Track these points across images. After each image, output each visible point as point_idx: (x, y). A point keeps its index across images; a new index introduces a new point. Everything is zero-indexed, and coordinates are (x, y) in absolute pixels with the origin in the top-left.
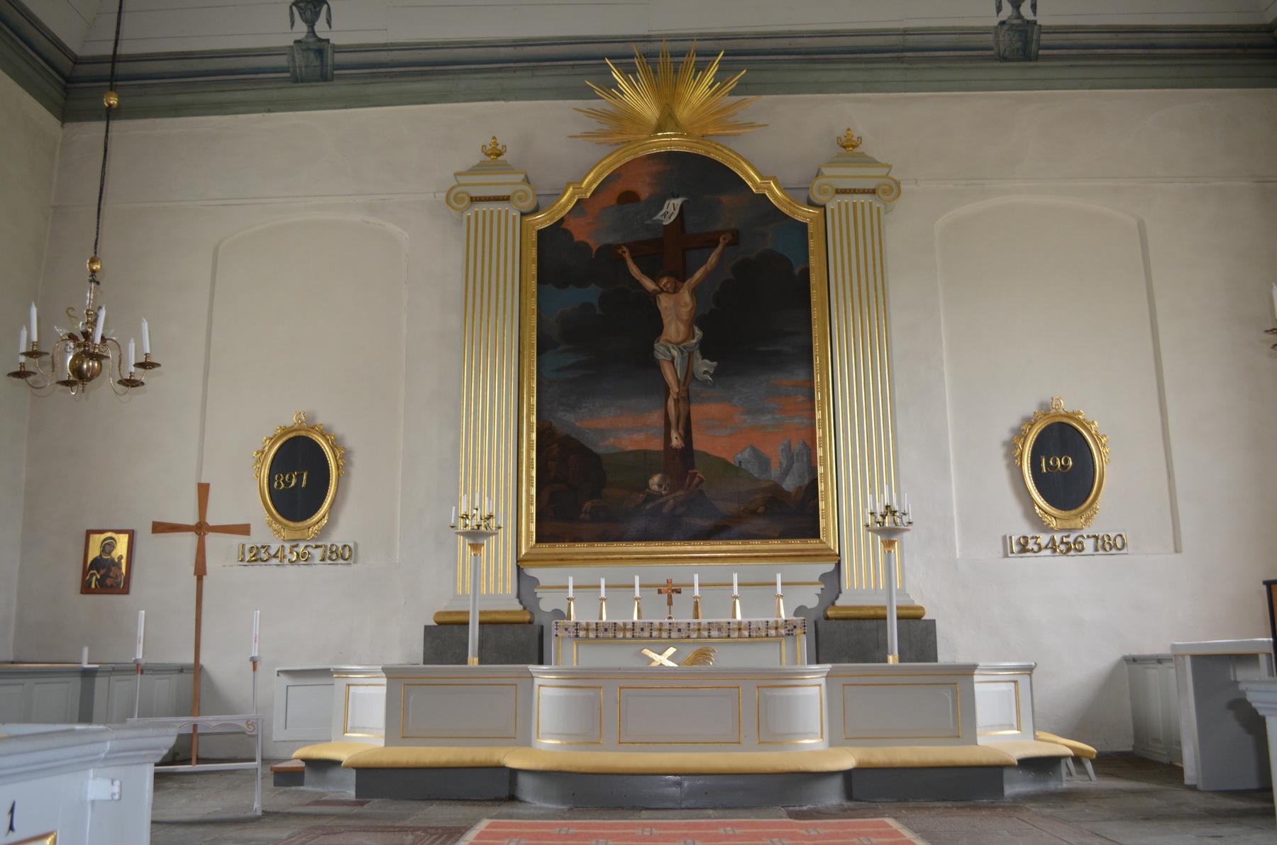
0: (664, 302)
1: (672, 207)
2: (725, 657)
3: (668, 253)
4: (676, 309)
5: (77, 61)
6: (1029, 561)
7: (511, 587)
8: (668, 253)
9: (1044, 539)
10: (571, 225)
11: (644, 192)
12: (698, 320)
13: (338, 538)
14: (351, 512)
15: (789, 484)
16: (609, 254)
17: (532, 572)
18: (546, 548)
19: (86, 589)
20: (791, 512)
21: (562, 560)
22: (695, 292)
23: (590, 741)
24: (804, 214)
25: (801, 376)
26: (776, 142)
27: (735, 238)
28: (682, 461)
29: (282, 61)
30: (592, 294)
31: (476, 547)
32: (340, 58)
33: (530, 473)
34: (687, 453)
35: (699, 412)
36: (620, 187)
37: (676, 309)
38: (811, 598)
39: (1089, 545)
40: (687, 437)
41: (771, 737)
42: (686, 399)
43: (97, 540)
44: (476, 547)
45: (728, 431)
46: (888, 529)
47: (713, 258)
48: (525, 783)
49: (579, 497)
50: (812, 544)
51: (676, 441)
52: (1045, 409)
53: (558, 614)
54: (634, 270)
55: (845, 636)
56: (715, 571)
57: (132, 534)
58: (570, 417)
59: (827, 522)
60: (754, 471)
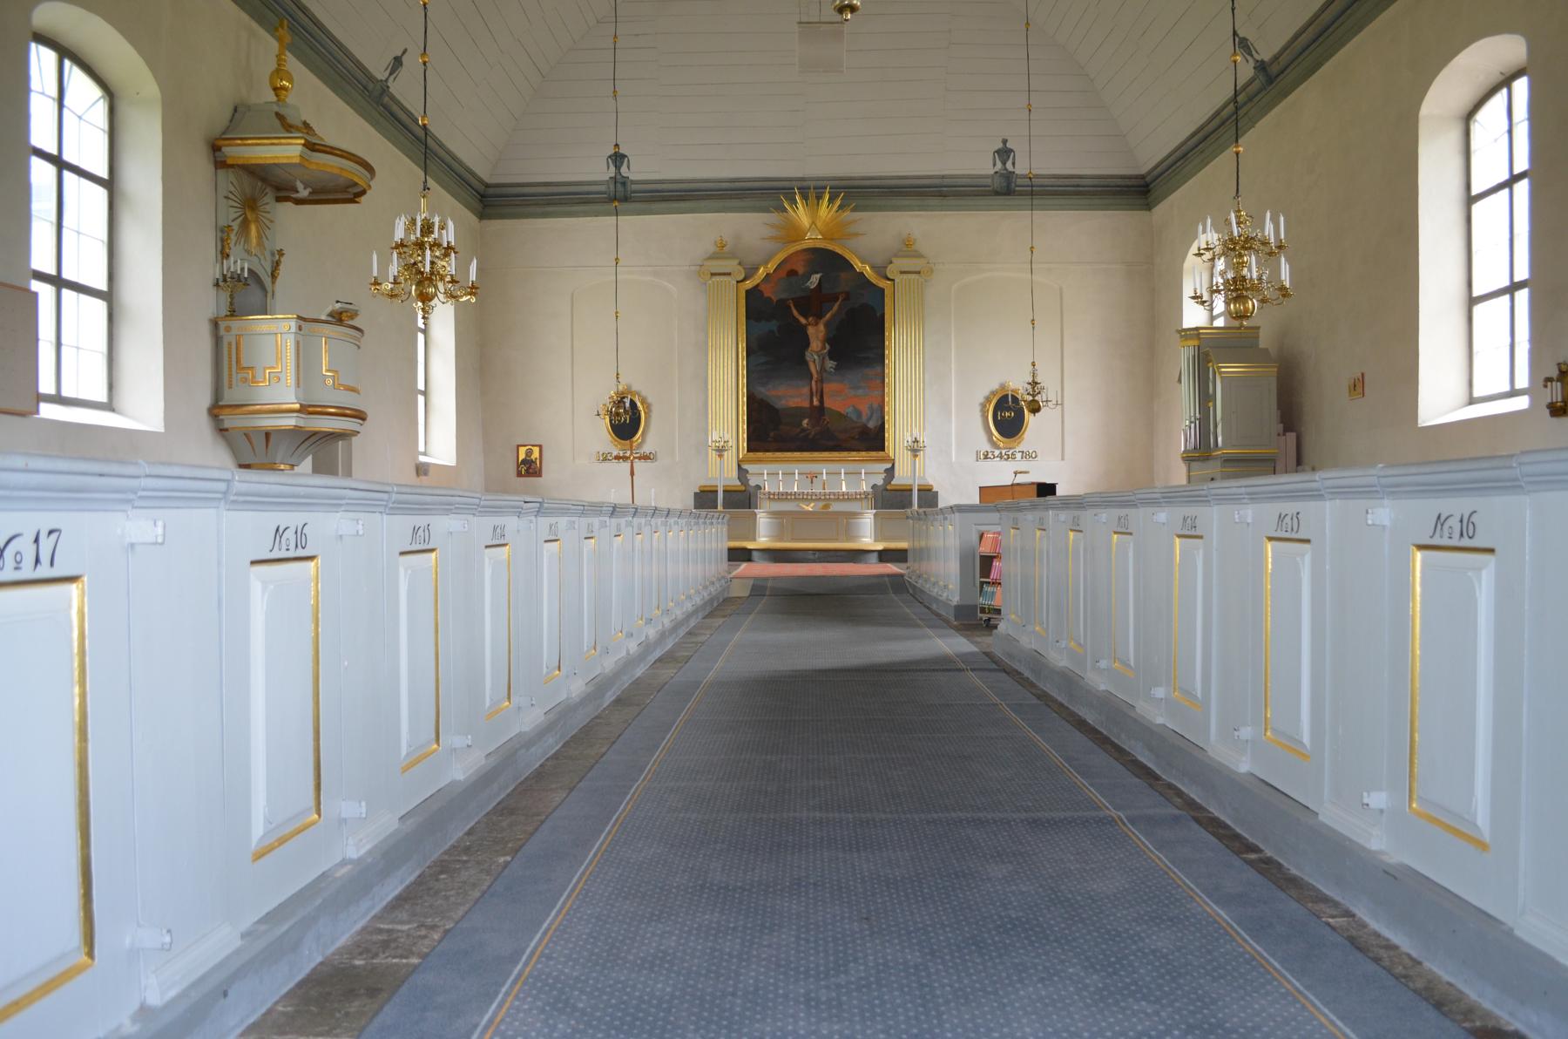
0: (811, 331)
1: (815, 278)
2: (836, 507)
3: (813, 304)
4: (817, 334)
5: (487, 186)
6: (988, 463)
7: (735, 474)
8: (813, 304)
9: (997, 453)
10: (762, 288)
11: (801, 270)
12: (828, 340)
13: (646, 449)
14: (651, 438)
15: (871, 425)
16: (782, 302)
17: (745, 466)
18: (751, 454)
19: (519, 474)
20: (871, 439)
21: (760, 461)
22: (827, 325)
23: (781, 540)
24: (882, 283)
25: (879, 369)
26: (871, 238)
27: (847, 296)
28: (819, 412)
29: (603, 188)
30: (773, 325)
31: (721, 456)
32: (634, 187)
33: (743, 418)
34: (821, 408)
35: (827, 388)
36: (788, 267)
37: (817, 334)
38: (879, 480)
39: (1019, 456)
40: (821, 401)
41: (851, 537)
42: (821, 381)
43: (523, 451)
44: (721, 456)
45: (841, 398)
46: (915, 449)
47: (836, 307)
48: (755, 554)
49: (769, 430)
50: (881, 454)
51: (816, 403)
52: (1003, 387)
53: (758, 487)
54: (795, 313)
55: (891, 499)
56: (833, 467)
57: (540, 447)
58: (762, 390)
59: (889, 443)
60: (854, 417)
